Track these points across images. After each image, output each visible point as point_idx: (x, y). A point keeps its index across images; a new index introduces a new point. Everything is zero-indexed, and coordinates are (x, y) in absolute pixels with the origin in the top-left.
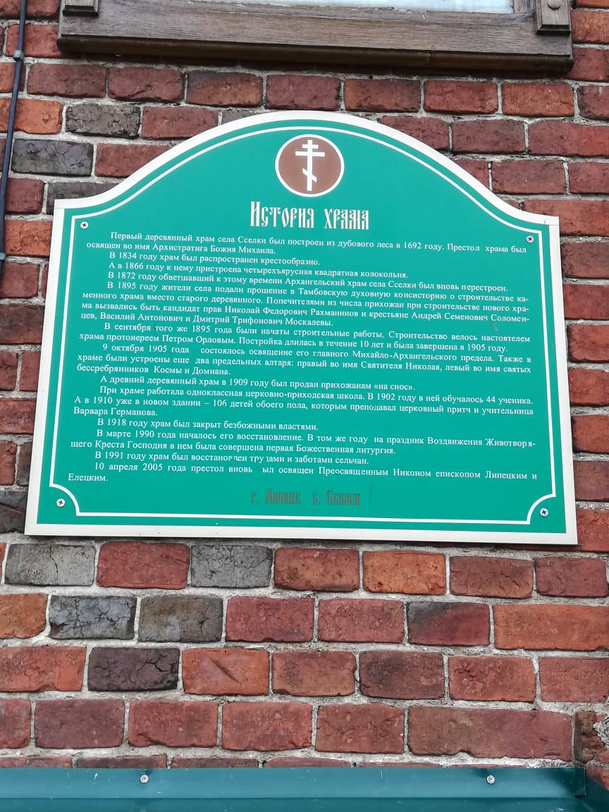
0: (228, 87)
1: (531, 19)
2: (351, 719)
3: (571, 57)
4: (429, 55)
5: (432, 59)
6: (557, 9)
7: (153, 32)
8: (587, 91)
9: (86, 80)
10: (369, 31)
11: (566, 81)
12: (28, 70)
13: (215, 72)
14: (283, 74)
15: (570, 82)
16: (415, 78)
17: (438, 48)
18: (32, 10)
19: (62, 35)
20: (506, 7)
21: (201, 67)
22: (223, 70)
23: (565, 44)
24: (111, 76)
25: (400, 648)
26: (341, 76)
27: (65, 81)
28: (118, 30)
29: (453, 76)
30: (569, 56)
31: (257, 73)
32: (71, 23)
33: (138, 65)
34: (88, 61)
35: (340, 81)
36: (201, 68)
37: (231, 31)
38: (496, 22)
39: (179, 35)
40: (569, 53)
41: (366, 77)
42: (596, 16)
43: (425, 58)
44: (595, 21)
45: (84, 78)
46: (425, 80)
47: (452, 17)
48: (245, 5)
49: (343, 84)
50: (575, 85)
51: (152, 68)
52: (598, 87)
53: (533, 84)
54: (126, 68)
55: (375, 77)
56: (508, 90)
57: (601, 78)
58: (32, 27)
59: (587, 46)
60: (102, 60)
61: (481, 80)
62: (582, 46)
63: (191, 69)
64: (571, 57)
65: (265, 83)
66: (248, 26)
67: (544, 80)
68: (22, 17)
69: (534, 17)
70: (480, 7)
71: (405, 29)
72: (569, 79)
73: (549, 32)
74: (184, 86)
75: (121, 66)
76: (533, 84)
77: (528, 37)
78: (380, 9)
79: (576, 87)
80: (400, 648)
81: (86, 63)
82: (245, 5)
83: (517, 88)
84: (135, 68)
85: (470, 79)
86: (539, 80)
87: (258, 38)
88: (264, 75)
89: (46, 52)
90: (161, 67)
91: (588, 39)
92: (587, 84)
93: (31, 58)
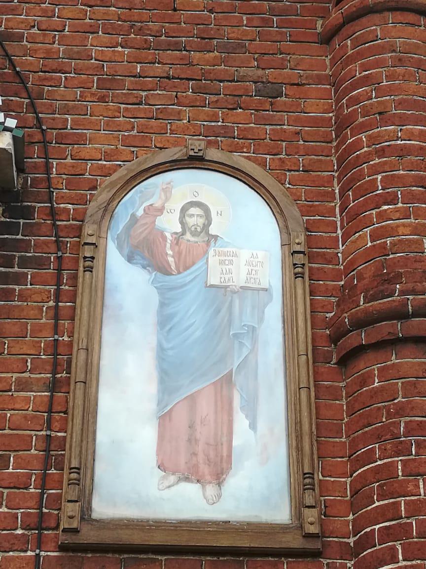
0: (145, 566)
1: (300, 529)
2: (134, 31)
3: (321, 549)
4: (248, 549)
5: (249, 551)
6: (313, 524)
7: (107, 540)
8: (330, 565)
9: (72, 564)
10: (218, 536)
11: (321, 559)
12: (42, 559)
13: (138, 557)
14: (173, 557)
15: (322, 560)
16: (241, 559)
17: (252, 545)
18: (44, 526)
19: (61, 543)
20: (288, 520)
21: (131, 555)
22: (142, 556)
23: (318, 542)
24: (85, 561)
25: (377, 463)
26: (203, 558)
27: (61, 565)
28: (90, 539)
29: (261, 557)
30: (320, 549)
31: (160, 558)
32: (66, 536)
33: (98, 555)
34: (73, 553)
35: (202, 561)
36: (131, 556)
37: (147, 538)
38: (283, 529)
39: (121, 541)
40: (319, 547)
41: (215, 559)
42: (336, 522)
43: (246, 550)
44: (336, 525)
45: (70, 563)
46: (247, 559)
47: (260, 527)
48: (153, 522)
49: (204, 562)
50: (325, 562)
51: (105, 556)
52: (337, 563)
53: (302, 561)
54: (91, 557)
55: (221, 558)
56: (289, 565)
57: (338, 558)
58: (43, 535)
59: (331, 539)
60: (80, 553)
61: (276, 559)
62: (328, 539)
63: (126, 556)
64: (321, 549)
65: (163, 563)
66: (155, 535)
67: (308, 559)
68: (39, 529)
69: (302, 527)
70: (275, 520)
71: (234, 535)
72: (321, 558)
73: (308, 536)
74: (122, 565)
75: (90, 555)
76: (302, 561)
77: (298, 538)
78: (223, 522)
79: (325, 563)
80: (377, 463)
81: (71, 554)
82: (153, 522)
83: (295, 564)
84: (97, 557)
85: (270, 559)
86: (306, 559)
87: (160, 542)
88: (164, 558)
89: (51, 549)
90: (110, 555)
91: (331, 536)
92: (331, 561)
93: (43, 552)
